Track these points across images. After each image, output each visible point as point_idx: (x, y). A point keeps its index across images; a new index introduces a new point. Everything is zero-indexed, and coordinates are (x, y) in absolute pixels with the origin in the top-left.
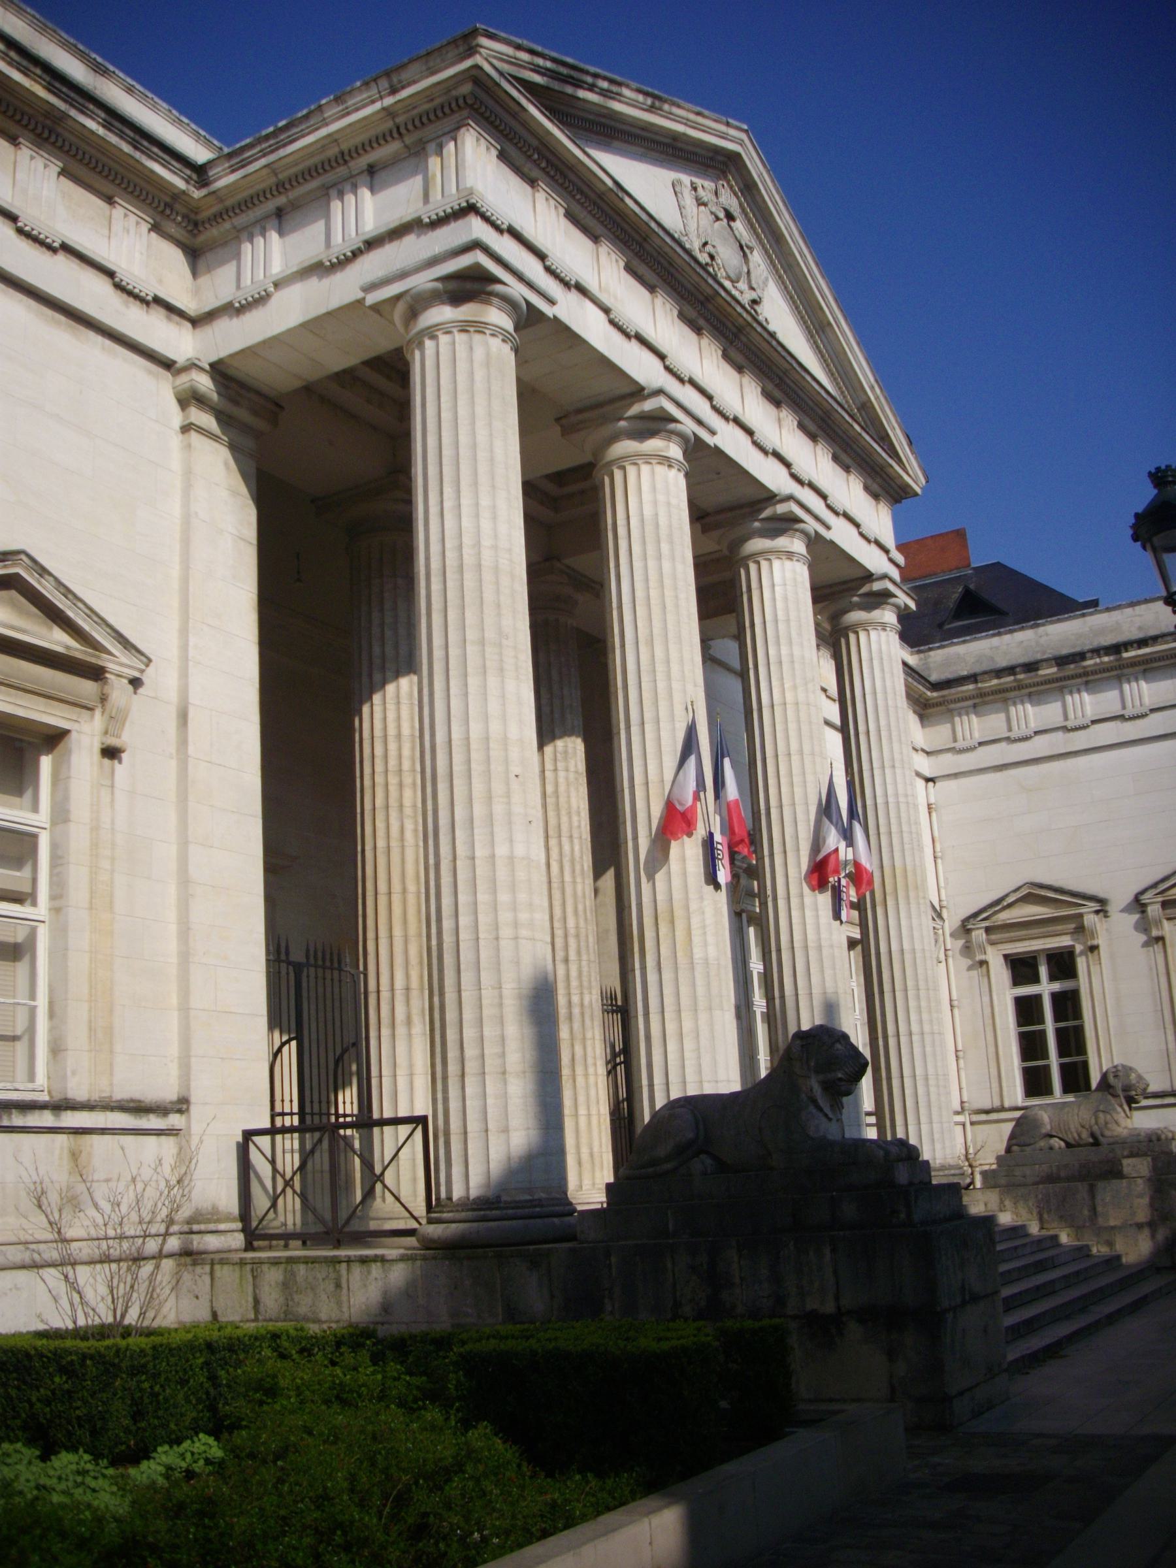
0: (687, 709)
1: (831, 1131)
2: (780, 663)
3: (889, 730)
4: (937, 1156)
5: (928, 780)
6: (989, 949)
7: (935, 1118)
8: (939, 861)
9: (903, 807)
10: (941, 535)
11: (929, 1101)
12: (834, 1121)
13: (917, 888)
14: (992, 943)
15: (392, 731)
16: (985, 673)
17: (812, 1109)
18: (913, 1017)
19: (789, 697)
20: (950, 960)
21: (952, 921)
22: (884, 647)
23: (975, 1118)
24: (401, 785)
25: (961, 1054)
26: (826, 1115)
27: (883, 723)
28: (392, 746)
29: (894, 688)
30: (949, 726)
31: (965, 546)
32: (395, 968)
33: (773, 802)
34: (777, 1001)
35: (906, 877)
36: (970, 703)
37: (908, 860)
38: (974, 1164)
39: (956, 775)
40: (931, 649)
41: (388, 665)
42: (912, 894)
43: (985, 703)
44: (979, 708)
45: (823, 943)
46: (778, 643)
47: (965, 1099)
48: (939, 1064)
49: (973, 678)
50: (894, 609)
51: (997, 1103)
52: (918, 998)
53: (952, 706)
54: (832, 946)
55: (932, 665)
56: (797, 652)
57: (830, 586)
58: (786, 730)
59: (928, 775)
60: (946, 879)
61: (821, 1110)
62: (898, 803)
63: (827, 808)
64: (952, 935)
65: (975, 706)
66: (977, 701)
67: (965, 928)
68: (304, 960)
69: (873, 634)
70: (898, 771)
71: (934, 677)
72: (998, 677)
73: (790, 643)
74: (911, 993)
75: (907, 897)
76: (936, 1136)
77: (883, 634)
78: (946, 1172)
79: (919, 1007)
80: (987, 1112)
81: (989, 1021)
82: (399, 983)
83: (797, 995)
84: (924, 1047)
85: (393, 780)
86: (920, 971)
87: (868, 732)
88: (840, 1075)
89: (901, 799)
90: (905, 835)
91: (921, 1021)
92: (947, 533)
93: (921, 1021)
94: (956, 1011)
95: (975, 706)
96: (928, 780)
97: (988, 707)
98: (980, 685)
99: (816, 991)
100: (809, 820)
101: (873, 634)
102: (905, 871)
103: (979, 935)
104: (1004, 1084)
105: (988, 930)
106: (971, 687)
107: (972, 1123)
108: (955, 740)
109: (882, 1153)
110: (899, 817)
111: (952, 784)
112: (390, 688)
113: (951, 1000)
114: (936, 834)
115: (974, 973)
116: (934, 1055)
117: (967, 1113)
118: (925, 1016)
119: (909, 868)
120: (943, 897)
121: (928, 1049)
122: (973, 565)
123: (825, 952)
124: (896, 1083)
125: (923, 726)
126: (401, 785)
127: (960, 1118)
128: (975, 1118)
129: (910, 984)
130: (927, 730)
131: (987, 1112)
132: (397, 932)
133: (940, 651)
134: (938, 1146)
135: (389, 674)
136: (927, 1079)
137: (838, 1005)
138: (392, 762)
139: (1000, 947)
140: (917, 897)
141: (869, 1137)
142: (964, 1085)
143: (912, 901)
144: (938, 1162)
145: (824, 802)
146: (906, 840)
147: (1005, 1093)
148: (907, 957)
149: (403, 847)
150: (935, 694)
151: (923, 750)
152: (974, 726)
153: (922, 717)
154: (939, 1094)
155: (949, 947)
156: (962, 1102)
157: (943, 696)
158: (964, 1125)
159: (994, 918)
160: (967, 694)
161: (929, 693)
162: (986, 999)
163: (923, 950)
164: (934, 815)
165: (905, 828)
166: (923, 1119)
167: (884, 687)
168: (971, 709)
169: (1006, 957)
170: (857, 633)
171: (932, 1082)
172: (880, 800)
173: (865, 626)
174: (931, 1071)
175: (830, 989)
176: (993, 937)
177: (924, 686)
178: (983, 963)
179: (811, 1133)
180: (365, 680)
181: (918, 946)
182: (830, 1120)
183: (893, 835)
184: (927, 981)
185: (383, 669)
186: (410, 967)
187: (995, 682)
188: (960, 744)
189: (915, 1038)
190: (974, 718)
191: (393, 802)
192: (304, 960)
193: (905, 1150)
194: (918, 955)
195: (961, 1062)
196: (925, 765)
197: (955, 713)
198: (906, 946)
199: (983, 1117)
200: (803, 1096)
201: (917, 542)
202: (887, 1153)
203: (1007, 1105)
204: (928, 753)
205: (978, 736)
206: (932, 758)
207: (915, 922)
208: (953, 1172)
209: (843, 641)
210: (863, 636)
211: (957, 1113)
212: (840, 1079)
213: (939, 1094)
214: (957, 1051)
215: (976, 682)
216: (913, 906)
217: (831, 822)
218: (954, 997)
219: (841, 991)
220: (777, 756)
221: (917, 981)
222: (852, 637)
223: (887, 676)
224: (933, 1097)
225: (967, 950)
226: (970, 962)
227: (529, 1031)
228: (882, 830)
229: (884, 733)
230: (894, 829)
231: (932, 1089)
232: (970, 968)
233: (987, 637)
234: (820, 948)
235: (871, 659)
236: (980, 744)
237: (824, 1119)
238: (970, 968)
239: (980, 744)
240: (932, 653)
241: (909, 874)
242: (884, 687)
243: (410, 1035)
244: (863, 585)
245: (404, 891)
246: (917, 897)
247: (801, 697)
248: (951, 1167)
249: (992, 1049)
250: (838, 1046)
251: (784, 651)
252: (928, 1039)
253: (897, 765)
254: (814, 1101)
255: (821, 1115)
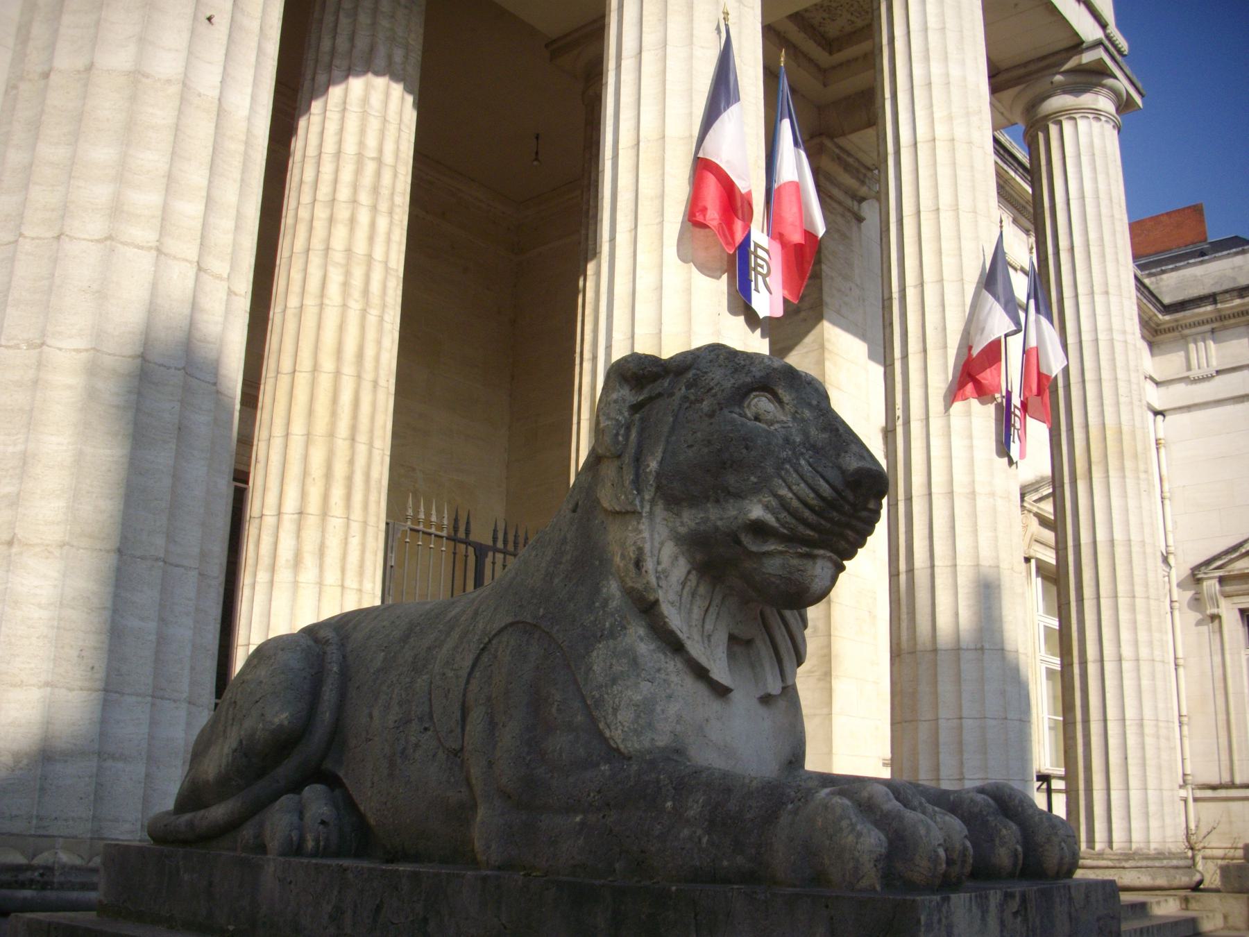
0: (718, 29)
1: (730, 740)
2: (929, 84)
3: (1102, 245)
4: (1152, 837)
5: (1157, 413)
6: (1223, 602)
7: (1152, 783)
8: (1167, 502)
9: (1119, 347)
10: (1178, 211)
11: (1144, 758)
12: (743, 699)
13: (1135, 456)
14: (1227, 596)
15: (329, 147)
16: (1226, 292)
17: (637, 638)
18: (1125, 635)
19: (941, 131)
20: (1176, 613)
21: (1181, 569)
22: (1097, 141)
23: (1199, 794)
24: (331, 220)
25: (1185, 720)
26: (700, 673)
27: (1093, 236)
28: (327, 168)
29: (1105, 153)
30: (1182, 353)
31: (1201, 221)
32: (287, 480)
33: (911, 279)
34: (903, 578)
35: (1121, 441)
36: (1208, 327)
37: (1125, 418)
38: (1198, 846)
39: (1188, 408)
40: (1163, 272)
41: (337, 62)
42: (1128, 464)
43: (1225, 328)
44: (1216, 334)
45: (978, 489)
46: (927, 58)
47: (1188, 771)
48: (1161, 705)
49: (1212, 298)
50: (1111, 95)
51: (1226, 779)
52: (1133, 609)
53: (1187, 332)
54: (992, 494)
55: (1164, 289)
56: (955, 72)
57: (1026, 64)
58: (935, 176)
59: (1158, 407)
60: (1175, 523)
61: (674, 645)
62: (1112, 340)
63: (993, 278)
64: (1179, 585)
65: (1213, 331)
66: (1215, 325)
67: (1195, 577)
68: (490, 543)
69: (1082, 124)
70: (1113, 299)
71: (1167, 300)
72: (1241, 297)
73: (946, 59)
74: (1122, 602)
75: (1122, 469)
76: (1152, 808)
77: (1096, 124)
78: (1165, 862)
79: (1134, 623)
80: (1214, 788)
81: (1219, 685)
82: (290, 505)
83: (932, 566)
84: (1139, 679)
85: (321, 213)
86: (1137, 571)
87: (1072, 249)
88: (757, 512)
89: (1116, 336)
90: (1121, 384)
91: (1136, 643)
92: (1184, 209)
93: (1136, 643)
94: (1181, 670)
95: (1213, 331)
96: (1157, 413)
97: (1228, 332)
98: (1219, 306)
99: (964, 562)
100: (964, 305)
101: (1082, 124)
102: (1120, 432)
103: (1211, 586)
104: (1236, 757)
105: (1222, 580)
106: (1209, 308)
107: (1195, 800)
108: (1189, 368)
109: (872, 840)
110: (1113, 360)
111: (1185, 417)
112: (335, 92)
113: (1176, 658)
114: (1164, 472)
115: (1204, 629)
116: (1154, 691)
117: (1189, 787)
118: (1142, 636)
119: (1125, 429)
120: (1170, 542)
121: (1145, 683)
122: (1210, 240)
123: (981, 503)
124: (1095, 728)
125: (1152, 354)
126: (331, 220)
127: (1183, 793)
128: (1199, 794)
129: (1122, 588)
130: (1157, 359)
131: (1214, 788)
132: (298, 428)
133: (1174, 274)
134: (1154, 823)
135: (336, 73)
136: (1141, 725)
137: (999, 586)
138: (324, 190)
139: (1236, 600)
140: (1137, 470)
141: (843, 766)
142: (1187, 755)
143: (1128, 473)
144: (1153, 846)
145: (988, 266)
146: (1122, 390)
147: (1236, 767)
148: (1120, 551)
149: (321, 306)
150: (1167, 318)
151: (1152, 379)
152: (1211, 353)
153: (1151, 345)
154: (1158, 749)
155: (1175, 598)
156: (1184, 775)
157: (1176, 320)
158: (1185, 801)
159: (1229, 567)
160: (1204, 317)
161: (1160, 316)
162: (1217, 659)
163: (1143, 542)
164: (1162, 451)
165: (1121, 374)
166: (1134, 783)
167: (1096, 191)
168: (1209, 335)
169: (1242, 611)
170: (1060, 123)
171: (1148, 730)
172: (1086, 337)
173: (1070, 113)
174: (1148, 713)
175: (986, 560)
176: (1228, 589)
177: (1154, 305)
178: (1215, 618)
179: (616, 735)
180: (307, 84)
181: (1135, 537)
182: (721, 692)
183: (1104, 384)
184: (1146, 585)
185: (329, 68)
186: (309, 481)
187: (1237, 302)
188: (1195, 373)
189: (1126, 665)
190: (1211, 344)
191: (317, 244)
192: (490, 543)
193: (1010, 831)
194: (1136, 549)
195: (1185, 728)
196: (1157, 397)
197: (1190, 339)
198: (1118, 536)
199: (1209, 793)
200: (613, 587)
201: (1152, 219)
202: (899, 844)
203: (1238, 781)
204: (1157, 384)
205: (1215, 364)
206: (1163, 389)
207: (1132, 503)
208: (1175, 862)
209: (1041, 135)
210: (1067, 126)
211: (1181, 787)
212: (758, 529)
213: (1158, 749)
214: (1180, 716)
215: (1215, 302)
216: (1130, 482)
217: (998, 300)
218: (1180, 654)
219: (1004, 566)
220: (918, 212)
221: (1132, 584)
222: (1053, 129)
223: (1101, 178)
224: (1150, 753)
225: (1197, 603)
226: (1199, 616)
227: (106, 454)
228: (1089, 376)
229: (1094, 249)
230: (1105, 375)
231: (1149, 741)
232: (1199, 623)
233: (1228, 256)
234: (973, 495)
235: (1079, 156)
236: (1218, 372)
237: (687, 685)
238: (1199, 623)
239: (1218, 372)
240: (1164, 276)
241: (1126, 437)
242: (1096, 191)
243: (296, 584)
244: (1069, 59)
245: (315, 368)
246: (1137, 470)
247: (960, 132)
248: (1171, 856)
249: (1222, 717)
250: (762, 403)
251: (936, 69)
252: (1145, 668)
253: (1111, 290)
254: (648, 609)
255: (672, 667)
